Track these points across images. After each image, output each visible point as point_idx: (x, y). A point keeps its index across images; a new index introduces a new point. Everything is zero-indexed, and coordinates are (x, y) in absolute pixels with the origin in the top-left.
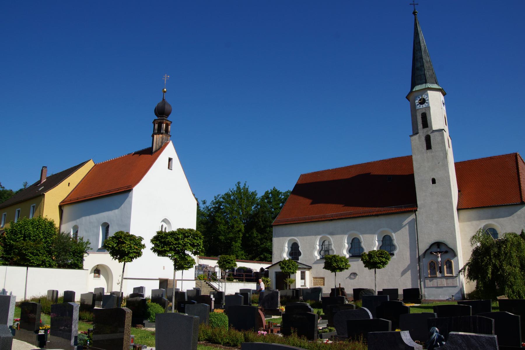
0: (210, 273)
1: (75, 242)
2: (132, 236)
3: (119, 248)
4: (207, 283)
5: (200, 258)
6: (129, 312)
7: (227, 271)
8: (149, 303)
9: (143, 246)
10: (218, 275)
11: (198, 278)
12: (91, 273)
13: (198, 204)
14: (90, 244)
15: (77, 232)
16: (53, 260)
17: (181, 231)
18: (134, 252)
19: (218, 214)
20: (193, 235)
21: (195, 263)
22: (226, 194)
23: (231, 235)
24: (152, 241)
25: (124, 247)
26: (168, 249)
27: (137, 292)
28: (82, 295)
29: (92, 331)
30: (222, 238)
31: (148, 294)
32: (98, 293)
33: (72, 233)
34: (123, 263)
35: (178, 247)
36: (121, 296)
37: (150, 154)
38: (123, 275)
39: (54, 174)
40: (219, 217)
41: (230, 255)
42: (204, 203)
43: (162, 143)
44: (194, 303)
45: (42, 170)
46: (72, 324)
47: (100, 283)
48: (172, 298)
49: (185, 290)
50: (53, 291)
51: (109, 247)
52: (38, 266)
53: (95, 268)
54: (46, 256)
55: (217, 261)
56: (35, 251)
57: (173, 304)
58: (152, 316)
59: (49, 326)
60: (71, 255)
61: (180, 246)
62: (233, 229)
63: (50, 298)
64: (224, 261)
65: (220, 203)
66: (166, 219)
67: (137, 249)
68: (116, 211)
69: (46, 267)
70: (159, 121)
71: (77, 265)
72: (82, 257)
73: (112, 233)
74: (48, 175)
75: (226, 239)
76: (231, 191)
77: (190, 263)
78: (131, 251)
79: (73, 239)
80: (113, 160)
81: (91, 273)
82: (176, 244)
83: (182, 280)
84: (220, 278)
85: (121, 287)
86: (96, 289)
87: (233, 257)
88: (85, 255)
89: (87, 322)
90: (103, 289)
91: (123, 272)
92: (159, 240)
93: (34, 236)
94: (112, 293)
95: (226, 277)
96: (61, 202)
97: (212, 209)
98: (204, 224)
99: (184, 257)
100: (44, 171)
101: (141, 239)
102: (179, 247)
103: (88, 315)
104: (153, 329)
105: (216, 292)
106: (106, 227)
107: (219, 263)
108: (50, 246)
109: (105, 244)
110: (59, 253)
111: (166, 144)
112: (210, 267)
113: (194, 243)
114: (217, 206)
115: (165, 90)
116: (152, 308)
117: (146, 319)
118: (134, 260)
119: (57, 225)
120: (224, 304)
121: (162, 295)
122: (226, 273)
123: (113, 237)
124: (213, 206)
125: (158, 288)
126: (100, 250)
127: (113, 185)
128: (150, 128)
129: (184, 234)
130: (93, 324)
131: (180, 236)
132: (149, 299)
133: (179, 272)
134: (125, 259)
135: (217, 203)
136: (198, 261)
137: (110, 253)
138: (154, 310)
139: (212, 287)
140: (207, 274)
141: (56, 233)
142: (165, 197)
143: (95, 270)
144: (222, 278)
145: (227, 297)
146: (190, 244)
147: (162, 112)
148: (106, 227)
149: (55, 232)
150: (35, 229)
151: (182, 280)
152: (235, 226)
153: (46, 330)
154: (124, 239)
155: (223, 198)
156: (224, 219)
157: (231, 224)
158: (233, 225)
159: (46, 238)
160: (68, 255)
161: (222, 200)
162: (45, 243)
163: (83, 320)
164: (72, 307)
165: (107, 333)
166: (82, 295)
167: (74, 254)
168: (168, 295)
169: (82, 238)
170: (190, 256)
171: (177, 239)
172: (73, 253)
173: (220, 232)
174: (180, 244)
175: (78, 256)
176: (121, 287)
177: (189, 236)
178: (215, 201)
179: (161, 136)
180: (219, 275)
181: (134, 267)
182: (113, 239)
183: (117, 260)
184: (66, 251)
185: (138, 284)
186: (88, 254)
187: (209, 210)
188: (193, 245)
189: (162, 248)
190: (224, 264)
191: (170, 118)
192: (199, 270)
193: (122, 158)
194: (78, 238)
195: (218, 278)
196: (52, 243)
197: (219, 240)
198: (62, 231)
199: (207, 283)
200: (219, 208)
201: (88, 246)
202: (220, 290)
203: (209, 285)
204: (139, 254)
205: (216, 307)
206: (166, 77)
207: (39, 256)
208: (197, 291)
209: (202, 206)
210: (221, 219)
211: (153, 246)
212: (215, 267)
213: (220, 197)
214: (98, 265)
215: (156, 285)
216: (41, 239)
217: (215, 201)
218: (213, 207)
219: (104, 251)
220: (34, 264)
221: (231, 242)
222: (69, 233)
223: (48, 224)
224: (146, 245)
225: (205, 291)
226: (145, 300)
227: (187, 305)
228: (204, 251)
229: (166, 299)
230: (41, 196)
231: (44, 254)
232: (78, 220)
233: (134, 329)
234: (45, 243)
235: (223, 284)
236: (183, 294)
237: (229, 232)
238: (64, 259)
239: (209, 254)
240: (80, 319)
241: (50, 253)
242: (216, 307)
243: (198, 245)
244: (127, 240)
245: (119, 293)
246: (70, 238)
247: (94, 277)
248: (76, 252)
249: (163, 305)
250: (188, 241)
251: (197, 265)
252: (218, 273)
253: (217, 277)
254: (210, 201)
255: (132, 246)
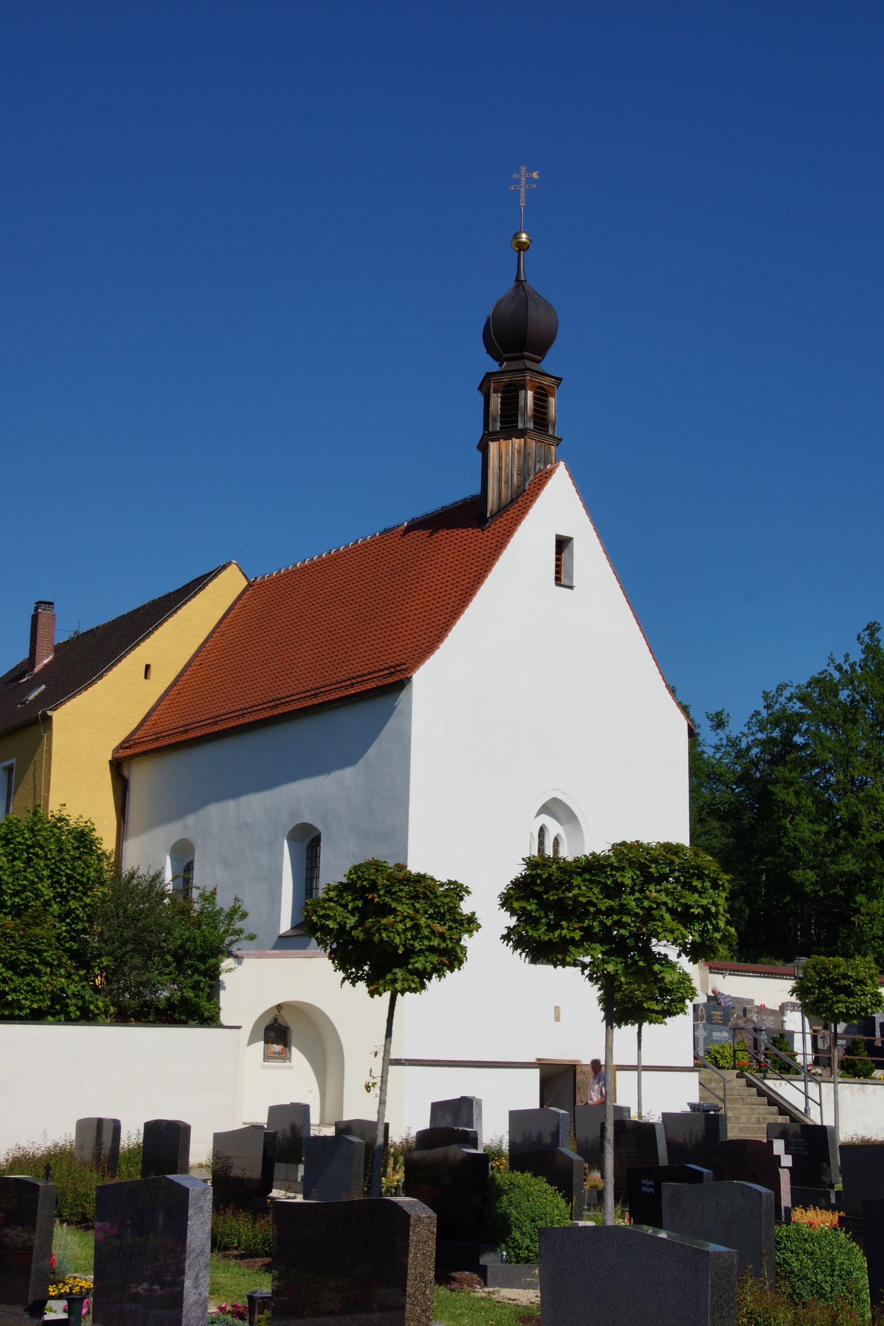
0: (763, 1037)
1: (185, 912)
2: (421, 878)
3: (367, 931)
4: (750, 1084)
5: (713, 970)
6: (421, 1214)
7: (841, 1027)
8: (501, 1172)
9: (470, 923)
10: (798, 1046)
11: (707, 1060)
12: (252, 1041)
13: (692, 734)
14: (244, 915)
15: (189, 868)
16: (96, 989)
17: (628, 854)
18: (432, 949)
19: (781, 771)
20: (683, 870)
21: (693, 992)
22: (814, 682)
23: (849, 864)
24: (507, 901)
25: (388, 930)
26: (577, 935)
27: (446, 1122)
28: (219, 1138)
29: (265, 1302)
30: (806, 876)
31: (493, 1131)
32: (283, 1127)
33: (168, 875)
34: (387, 995)
35: (619, 924)
36: (380, 1140)
37: (476, 525)
38: (387, 1051)
39: (84, 629)
40: (789, 783)
41: (848, 956)
42: (719, 722)
43: (523, 473)
44: (697, 1178)
45: (35, 618)
46: (182, 1272)
47: (292, 1082)
48: (601, 1149)
49: (653, 1114)
50: (100, 1121)
51: (325, 930)
52: (36, 1017)
53: (268, 1021)
54: (69, 976)
55: (790, 984)
56: (23, 956)
57: (605, 1178)
58: (516, 1234)
59: (86, 1281)
60: (167, 965)
61: (626, 919)
62: (855, 835)
63: (88, 1155)
64: (822, 984)
65: (789, 723)
66: (555, 801)
67: (442, 936)
68: (347, 775)
69: (69, 1020)
70: (506, 379)
71: (195, 1008)
72: (213, 974)
73: (333, 870)
74: (62, 637)
75: (825, 882)
76: (839, 668)
77: (669, 991)
78: (417, 945)
79: (174, 901)
80: (321, 562)
81: (252, 1041)
82: (609, 912)
83: (638, 1068)
84: (810, 1059)
85: (382, 1103)
86: (274, 1111)
87: (863, 965)
88: (227, 963)
89: (241, 1257)
90: (303, 1110)
91: (389, 1034)
92: (538, 896)
93: (16, 894)
94: (344, 1128)
95: (837, 1055)
96: (121, 747)
97: (755, 751)
98: (722, 817)
99: (648, 969)
100: (42, 620)
101: (457, 891)
102: (623, 925)
103: (245, 1229)
104: (528, 1296)
105: (796, 1127)
106: (308, 844)
107: (800, 991)
108: (84, 931)
109: (308, 917)
110: (121, 961)
111: (544, 478)
112: (762, 1009)
113: (687, 907)
114: (776, 734)
115: (524, 237)
116: (515, 1195)
117: (493, 1246)
118: (434, 984)
119: (108, 844)
120: (839, 1187)
121: (556, 1135)
122: (836, 1036)
123: (342, 888)
124: (760, 736)
125: (535, 1104)
126: (285, 943)
127: (331, 665)
128: (469, 413)
129: (643, 868)
130: (268, 1268)
131: (627, 878)
132: (499, 1154)
133: (626, 1033)
134: (394, 981)
135: (776, 723)
136: (705, 983)
137: (333, 956)
138: (525, 1204)
139: (773, 1100)
140: (749, 1042)
141: (106, 876)
142: (552, 710)
143: (268, 1029)
144: (816, 1062)
145: (848, 1149)
146: (672, 911)
147: (516, 340)
148: (308, 844)
149: (100, 871)
150: (19, 864)
151: (638, 1068)
152: (865, 821)
153: (74, 1301)
154: (389, 892)
155: (803, 699)
156: (811, 792)
157: (844, 813)
158: (856, 816)
159: (63, 898)
160: (155, 966)
161: (797, 706)
162: (61, 918)
163: (226, 1248)
164: (183, 1193)
165: (330, 1313)
166: (219, 1138)
167: (179, 960)
168: (581, 1135)
169: (214, 893)
170: (672, 966)
171: (614, 890)
172: (175, 956)
173: (795, 850)
174: (629, 913)
175: (197, 970)
176: (382, 1103)
177: (664, 877)
178: (764, 713)
179: (517, 442)
180: (802, 1048)
181: (435, 1013)
182: (340, 896)
183: (362, 985)
184: (148, 951)
185: (451, 1086)
186: (239, 959)
187: (741, 754)
188: (685, 917)
189: (551, 928)
190: (824, 999)
191: (550, 363)
192: (710, 1020)
193: (357, 548)
194: (195, 894)
195: (799, 1059)
196: (90, 919)
197: (795, 889)
198: (127, 866)
199: (750, 1084)
200: (787, 744)
201: (238, 925)
202: (815, 1117)
203: (761, 1093)
204: (451, 958)
205: (799, 1200)
206: (526, 178)
207: (38, 974)
208: (707, 1119)
209: (709, 738)
210: (797, 794)
211: (513, 922)
212: (783, 1007)
213: (787, 693)
214: (279, 1007)
215: (526, 1092)
216: (47, 904)
217: (764, 713)
218: (757, 743)
219: (304, 947)
220: (21, 1008)
221: (850, 896)
222: (158, 876)
223: (69, 841)
224: (481, 918)
225: (745, 1122)
226: (483, 1160)
227: (668, 1188)
228: (735, 940)
229: (575, 1157)
230: (39, 724)
231: (60, 966)
232: (191, 819)
233: (443, 1291)
234: (61, 918)
235: (827, 1088)
236: (646, 1130)
237: (839, 850)
238: (140, 984)
239: (755, 949)
240: (218, 1244)
241: (82, 960)
242: (799, 1200)
243: (708, 915)
244: (398, 900)
245: (372, 1125)
246: (163, 895)
247: (267, 1057)
248: (187, 954)
249: (563, 1180)
250: (663, 897)
251: (701, 999)
252: (798, 1038)
253: (793, 1055)
254: (743, 713)
255: (423, 921)
